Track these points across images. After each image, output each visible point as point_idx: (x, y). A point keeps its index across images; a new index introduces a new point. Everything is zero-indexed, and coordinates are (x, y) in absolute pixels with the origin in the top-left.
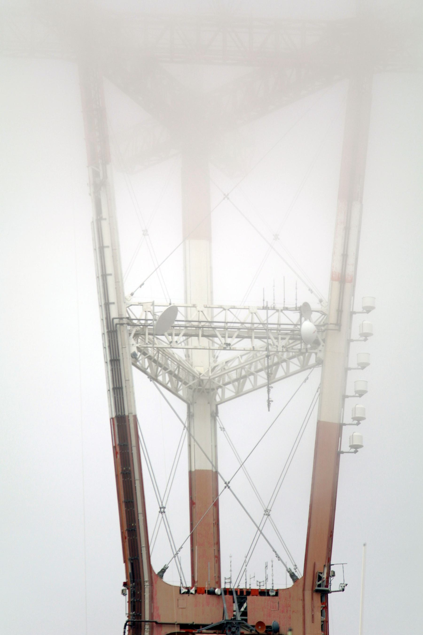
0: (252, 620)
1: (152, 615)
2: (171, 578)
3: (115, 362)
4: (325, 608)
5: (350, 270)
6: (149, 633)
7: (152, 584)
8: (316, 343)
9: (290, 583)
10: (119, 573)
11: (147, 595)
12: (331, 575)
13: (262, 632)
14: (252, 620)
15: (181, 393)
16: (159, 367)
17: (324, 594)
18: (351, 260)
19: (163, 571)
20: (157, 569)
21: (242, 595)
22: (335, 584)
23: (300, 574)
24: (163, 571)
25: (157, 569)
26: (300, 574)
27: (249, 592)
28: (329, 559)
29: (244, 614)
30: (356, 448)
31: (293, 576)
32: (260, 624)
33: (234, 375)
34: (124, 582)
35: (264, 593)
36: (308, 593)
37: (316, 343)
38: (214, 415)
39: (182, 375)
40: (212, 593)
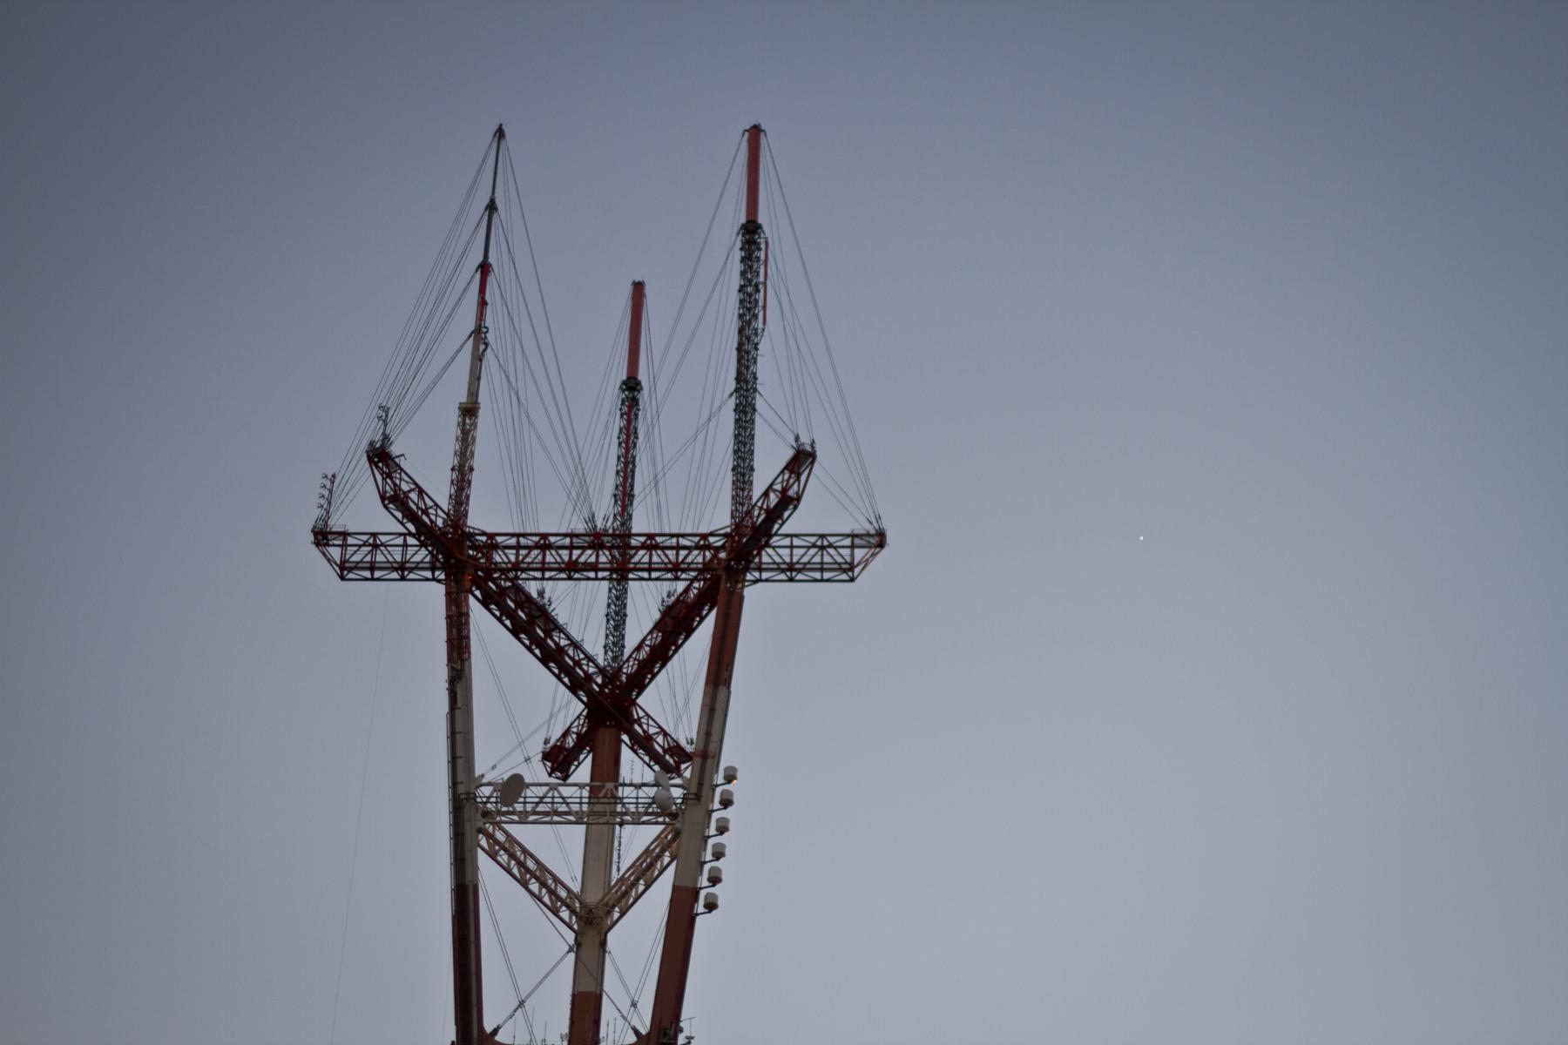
5: (712, 747)
18: (715, 738)
19: (495, 1031)
24: (495, 1031)
25: (489, 1028)
30: (711, 906)
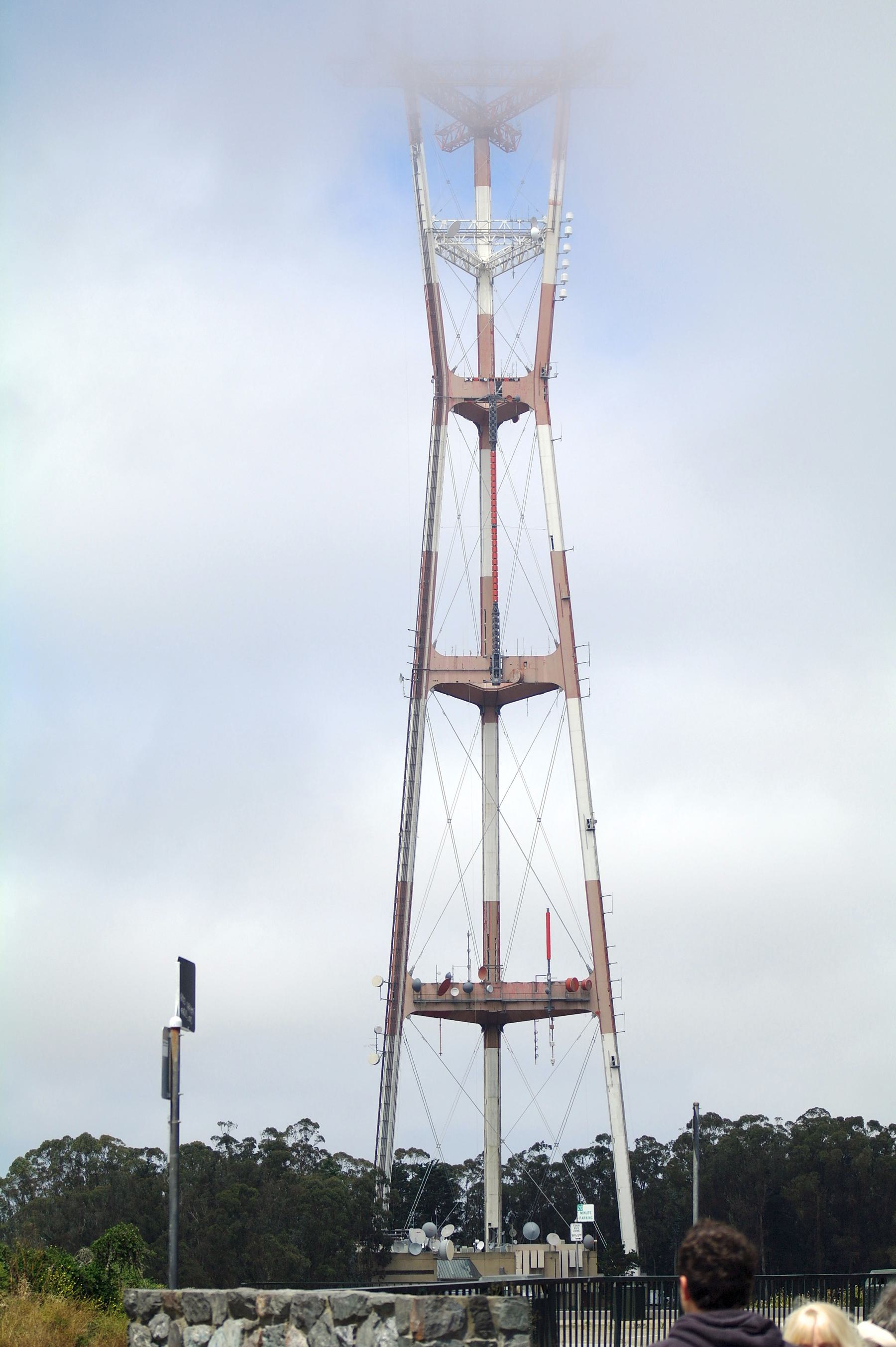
0: (504, 395)
1: (448, 393)
2: (459, 373)
3: (426, 254)
4: (546, 387)
6: (534, 1340)
7: (448, 376)
8: (541, 239)
9: (526, 374)
10: (430, 371)
11: (445, 382)
12: (549, 369)
13: (510, 401)
14: (504, 395)
15: (471, 271)
16: (457, 257)
17: (545, 380)
19: (455, 369)
20: (451, 368)
21: (499, 382)
22: (552, 374)
23: (532, 369)
24: (455, 369)
25: (451, 368)
26: (532, 369)
27: (503, 380)
28: (548, 360)
29: (501, 391)
31: (528, 369)
32: (509, 397)
33: (500, 261)
34: (575, 979)
35: (511, 380)
36: (537, 379)
37: (541, 239)
38: (492, 284)
39: (471, 260)
40: (482, 380)
